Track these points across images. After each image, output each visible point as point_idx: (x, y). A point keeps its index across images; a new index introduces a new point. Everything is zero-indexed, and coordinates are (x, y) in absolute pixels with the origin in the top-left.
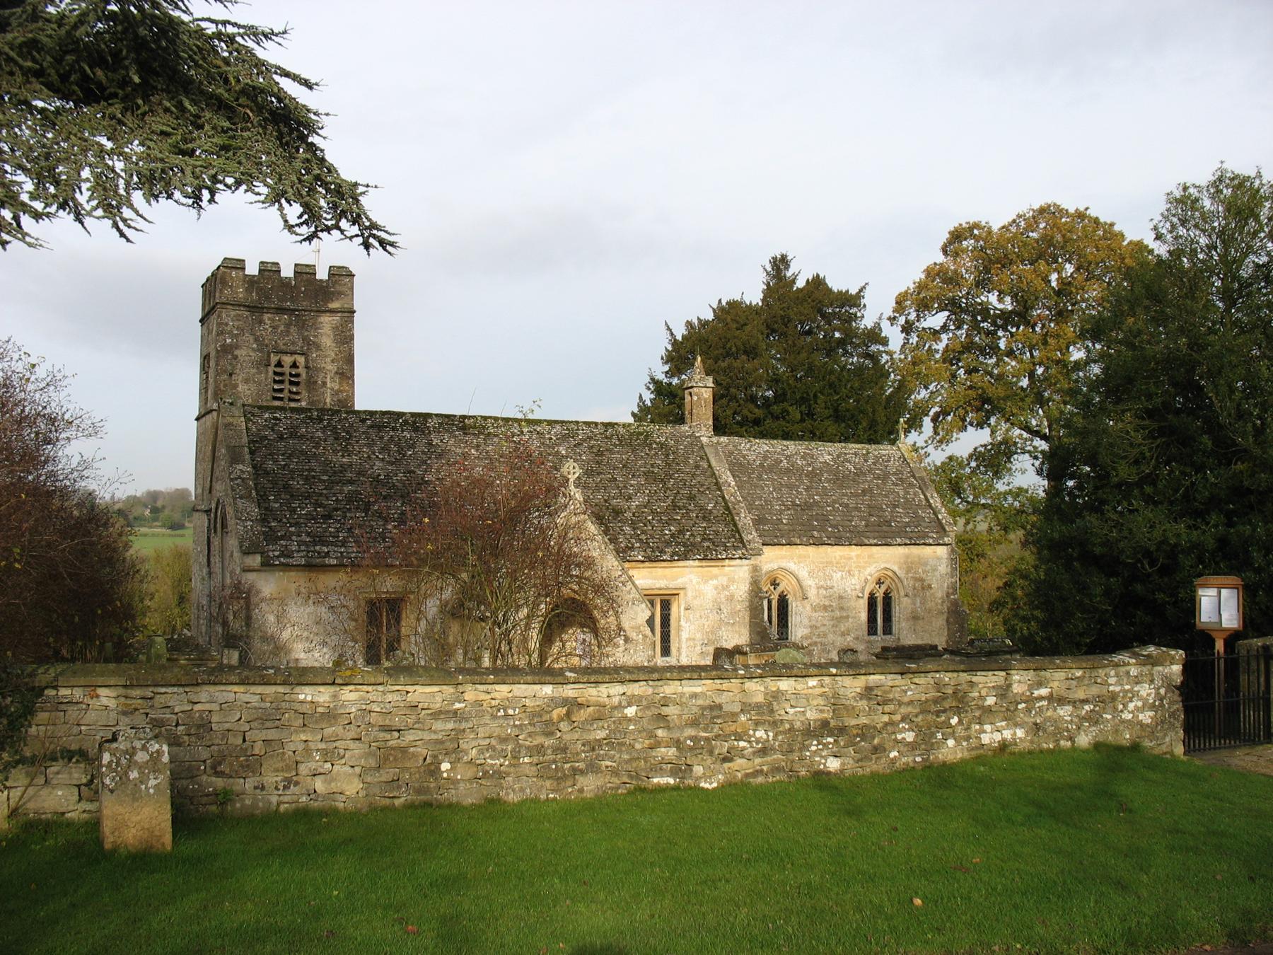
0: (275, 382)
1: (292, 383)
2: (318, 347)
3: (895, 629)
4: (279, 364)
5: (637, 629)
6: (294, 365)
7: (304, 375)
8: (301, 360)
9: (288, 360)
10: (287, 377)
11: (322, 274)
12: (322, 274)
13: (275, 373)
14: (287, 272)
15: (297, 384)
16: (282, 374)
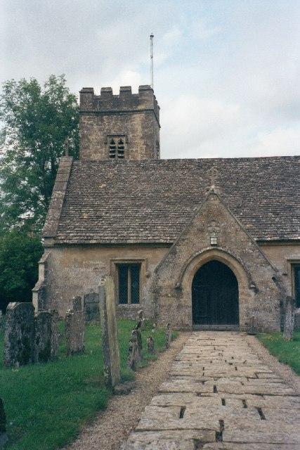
0: (111, 152)
1: (120, 152)
2: (133, 131)
3: (141, 298)
4: (113, 142)
5: (264, 283)
6: (121, 143)
7: (126, 148)
8: (124, 140)
9: (117, 140)
10: (117, 149)
11: (135, 91)
12: (135, 91)
13: (111, 148)
14: (116, 92)
15: (122, 152)
16: (114, 147)
